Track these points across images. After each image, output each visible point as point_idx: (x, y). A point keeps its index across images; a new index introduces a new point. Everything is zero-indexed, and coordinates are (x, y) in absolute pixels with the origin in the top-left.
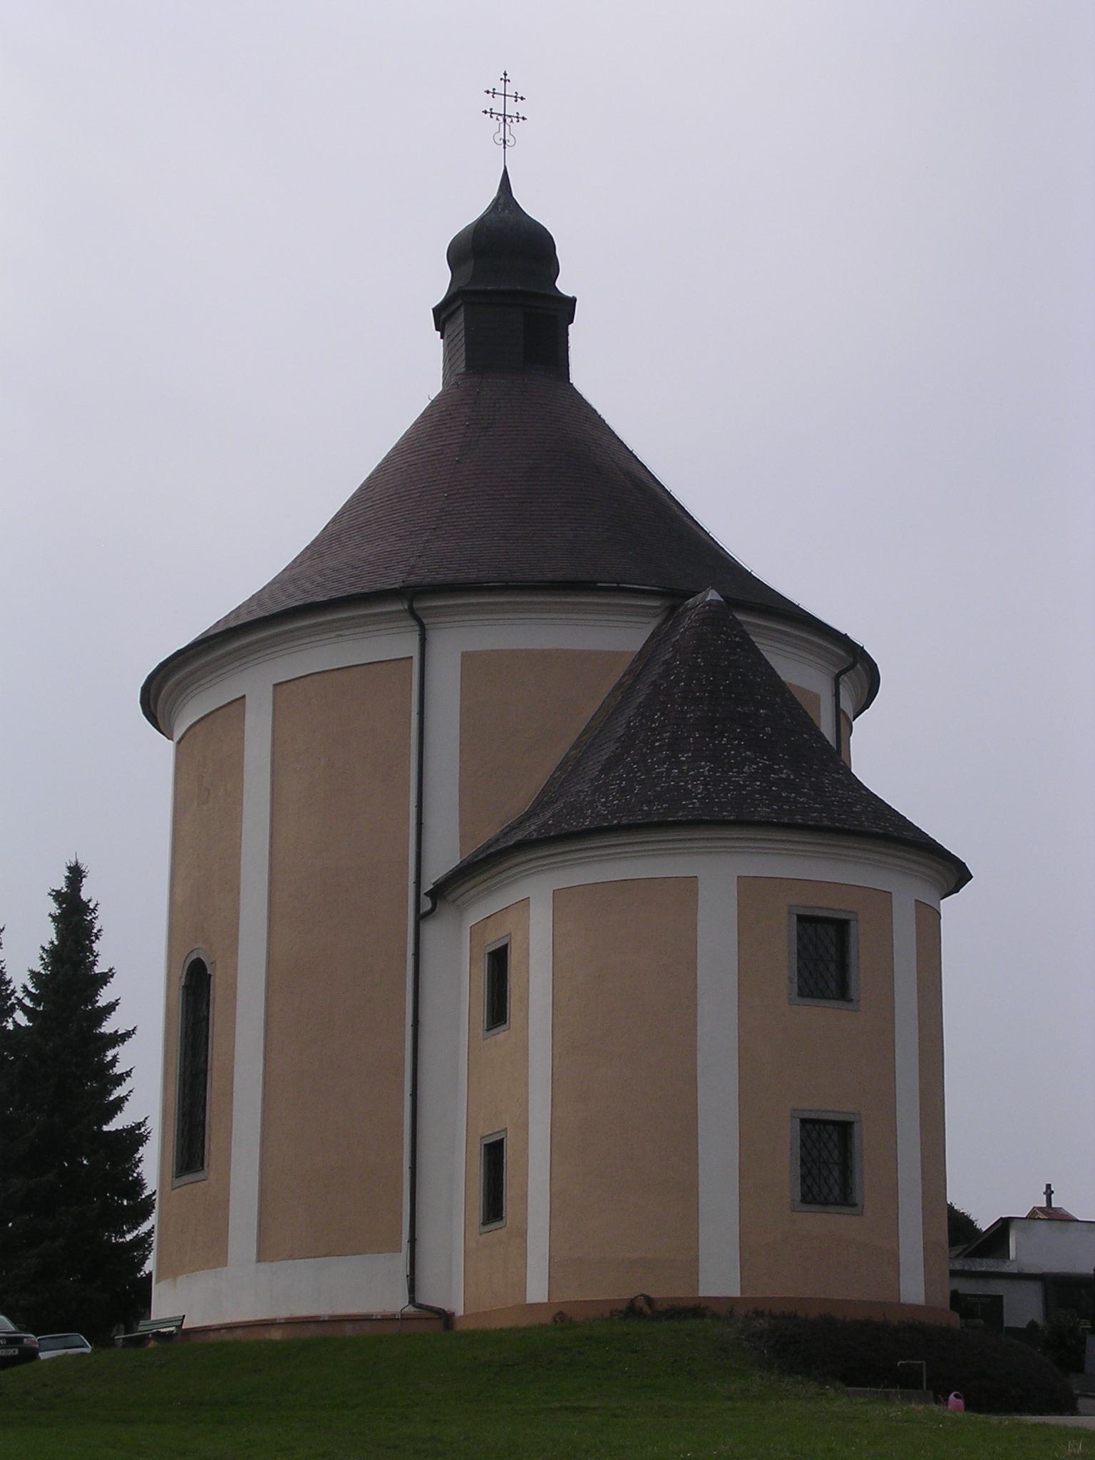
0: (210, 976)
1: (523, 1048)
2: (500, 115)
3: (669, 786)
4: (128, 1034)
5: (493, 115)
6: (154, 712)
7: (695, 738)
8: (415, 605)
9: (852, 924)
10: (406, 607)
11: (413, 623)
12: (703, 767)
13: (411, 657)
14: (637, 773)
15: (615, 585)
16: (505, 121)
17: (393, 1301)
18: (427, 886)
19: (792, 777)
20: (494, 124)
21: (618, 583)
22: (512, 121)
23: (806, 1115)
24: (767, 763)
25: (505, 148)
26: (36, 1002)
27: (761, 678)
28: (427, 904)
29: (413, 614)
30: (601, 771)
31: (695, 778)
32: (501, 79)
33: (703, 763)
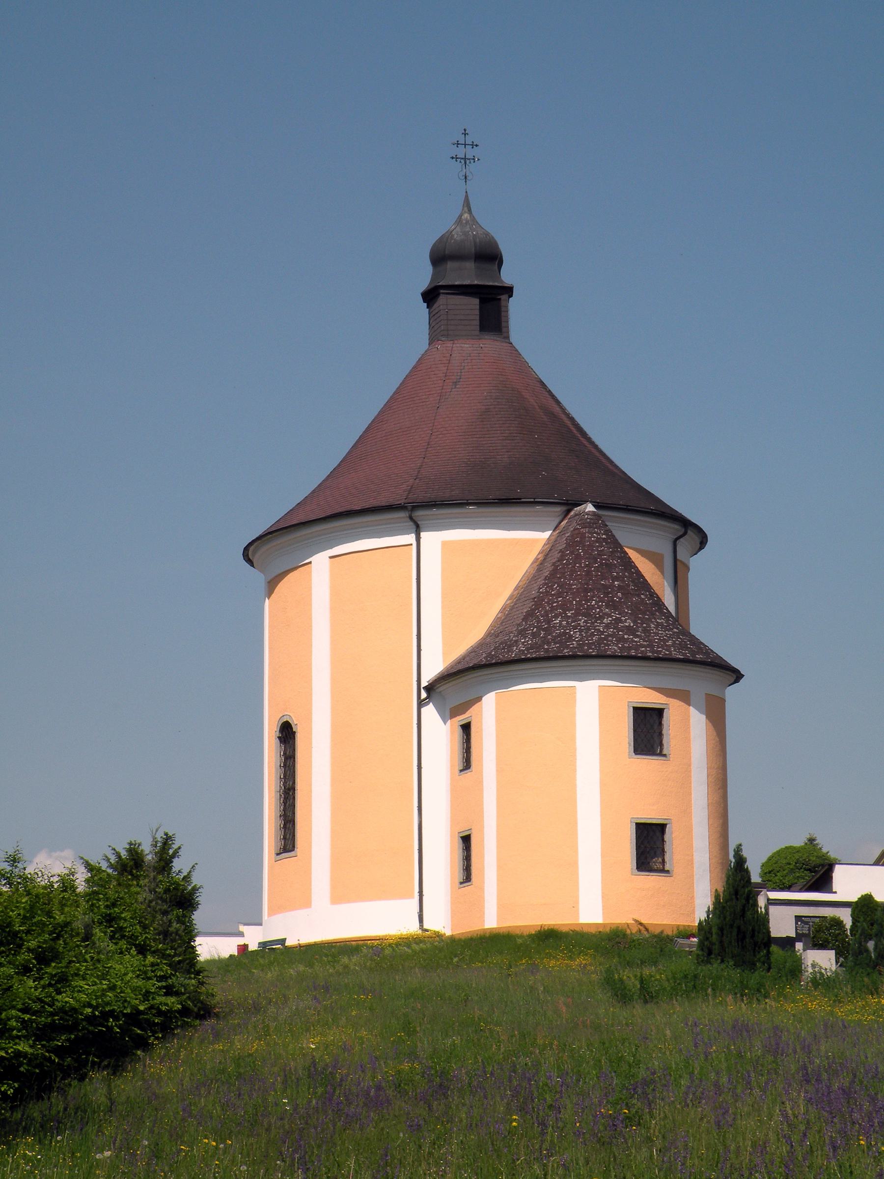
0: (295, 732)
1: (480, 783)
2: (462, 159)
3: (560, 633)
7: (576, 601)
11: (411, 523)
12: (580, 620)
13: (411, 545)
14: (542, 622)
15: (533, 500)
16: (465, 163)
17: (410, 927)
18: (424, 683)
19: (632, 624)
20: (458, 165)
21: (534, 499)
24: (618, 616)
27: (617, 561)
28: (424, 695)
30: (523, 620)
31: (575, 627)
33: (580, 617)
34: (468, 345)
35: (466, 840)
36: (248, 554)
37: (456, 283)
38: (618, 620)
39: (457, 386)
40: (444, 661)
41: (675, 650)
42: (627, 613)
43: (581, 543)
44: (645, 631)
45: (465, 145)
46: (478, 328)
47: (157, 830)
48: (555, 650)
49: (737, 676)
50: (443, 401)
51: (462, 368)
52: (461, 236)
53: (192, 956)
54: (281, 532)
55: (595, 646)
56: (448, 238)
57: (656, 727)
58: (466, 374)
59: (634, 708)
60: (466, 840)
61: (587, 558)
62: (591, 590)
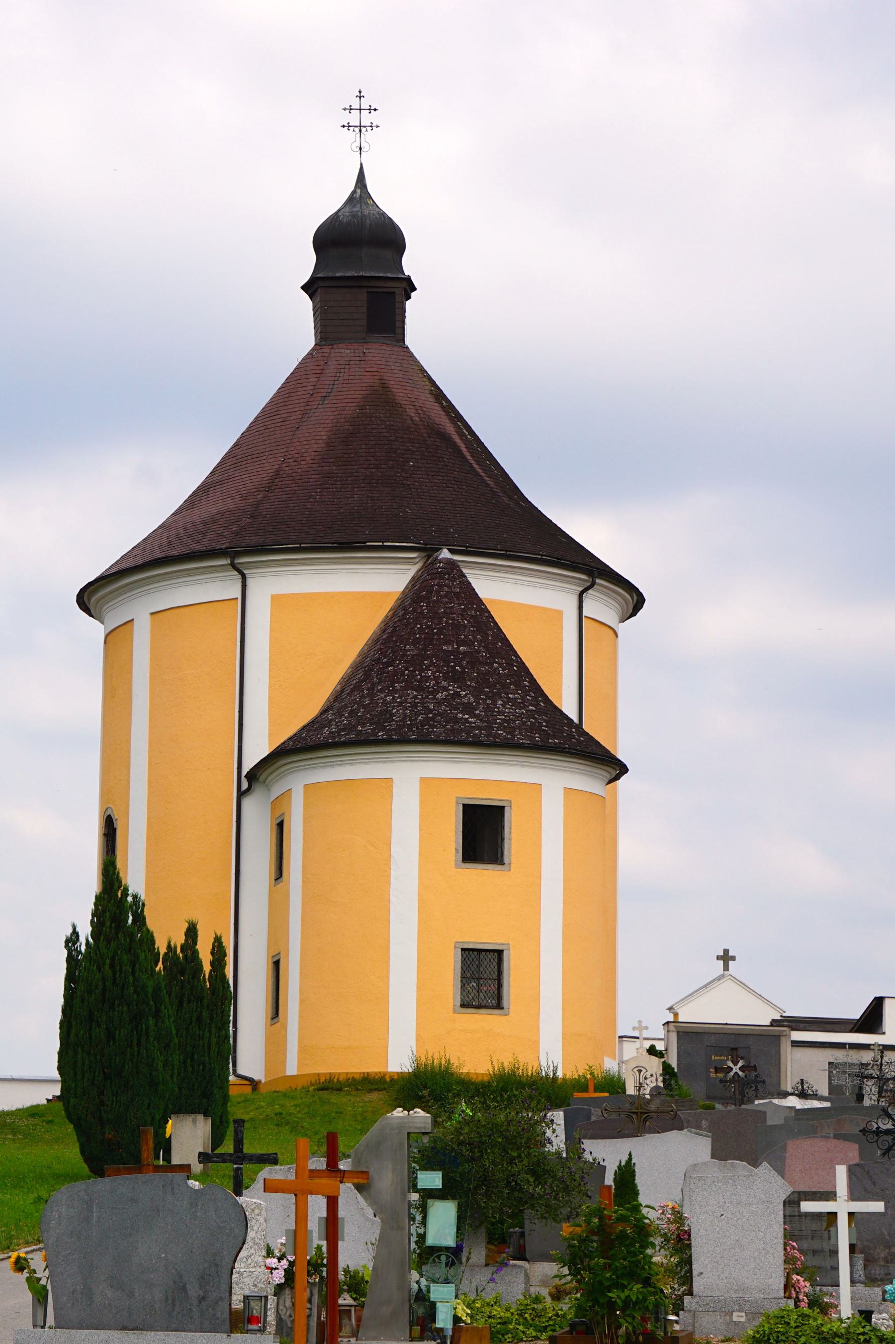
2: (356, 126)
4: (630, 1155)
5: (350, 128)
6: (87, 603)
8: (236, 561)
9: (506, 809)
10: (229, 562)
13: (237, 598)
16: (360, 131)
20: (352, 135)
22: (367, 131)
23: (466, 946)
25: (361, 154)
26: (534, 1151)
28: (245, 785)
29: (234, 566)
32: (357, 96)
34: (349, 351)
35: (277, 964)
36: (83, 600)
38: (457, 694)
39: (326, 402)
40: (270, 744)
41: (520, 734)
42: (470, 686)
43: (427, 598)
44: (487, 709)
45: (360, 109)
48: (368, 733)
49: (623, 769)
50: (305, 420)
51: (337, 378)
52: (347, 217)
55: (418, 728)
56: (362, 219)
58: (339, 386)
59: (464, 805)
60: (277, 964)
61: (430, 617)
62: (429, 658)
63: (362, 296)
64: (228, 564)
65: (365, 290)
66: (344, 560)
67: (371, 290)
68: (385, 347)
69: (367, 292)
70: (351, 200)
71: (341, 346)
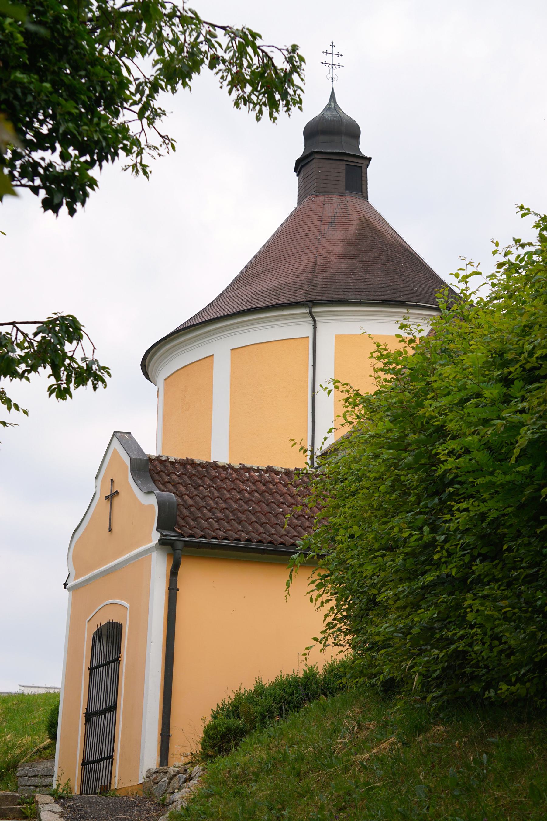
13: (309, 337)
16: (332, 67)
20: (327, 69)
29: (311, 314)
37: (328, 151)
46: (344, 187)
47: (240, 689)
53: (111, 624)
54: (164, 342)
57: (214, 473)
63: (342, 166)
64: (307, 313)
65: (345, 163)
66: (392, 314)
67: (348, 163)
68: (357, 199)
69: (346, 164)
70: (327, 108)
71: (330, 196)
